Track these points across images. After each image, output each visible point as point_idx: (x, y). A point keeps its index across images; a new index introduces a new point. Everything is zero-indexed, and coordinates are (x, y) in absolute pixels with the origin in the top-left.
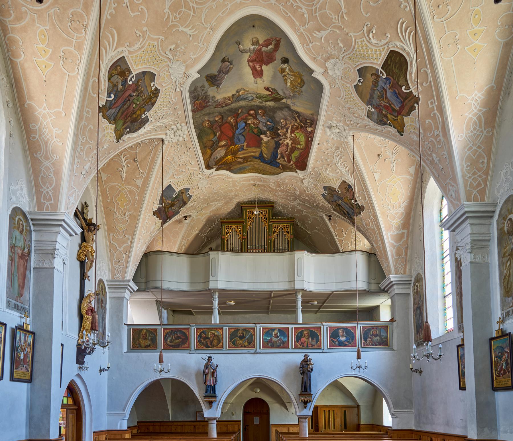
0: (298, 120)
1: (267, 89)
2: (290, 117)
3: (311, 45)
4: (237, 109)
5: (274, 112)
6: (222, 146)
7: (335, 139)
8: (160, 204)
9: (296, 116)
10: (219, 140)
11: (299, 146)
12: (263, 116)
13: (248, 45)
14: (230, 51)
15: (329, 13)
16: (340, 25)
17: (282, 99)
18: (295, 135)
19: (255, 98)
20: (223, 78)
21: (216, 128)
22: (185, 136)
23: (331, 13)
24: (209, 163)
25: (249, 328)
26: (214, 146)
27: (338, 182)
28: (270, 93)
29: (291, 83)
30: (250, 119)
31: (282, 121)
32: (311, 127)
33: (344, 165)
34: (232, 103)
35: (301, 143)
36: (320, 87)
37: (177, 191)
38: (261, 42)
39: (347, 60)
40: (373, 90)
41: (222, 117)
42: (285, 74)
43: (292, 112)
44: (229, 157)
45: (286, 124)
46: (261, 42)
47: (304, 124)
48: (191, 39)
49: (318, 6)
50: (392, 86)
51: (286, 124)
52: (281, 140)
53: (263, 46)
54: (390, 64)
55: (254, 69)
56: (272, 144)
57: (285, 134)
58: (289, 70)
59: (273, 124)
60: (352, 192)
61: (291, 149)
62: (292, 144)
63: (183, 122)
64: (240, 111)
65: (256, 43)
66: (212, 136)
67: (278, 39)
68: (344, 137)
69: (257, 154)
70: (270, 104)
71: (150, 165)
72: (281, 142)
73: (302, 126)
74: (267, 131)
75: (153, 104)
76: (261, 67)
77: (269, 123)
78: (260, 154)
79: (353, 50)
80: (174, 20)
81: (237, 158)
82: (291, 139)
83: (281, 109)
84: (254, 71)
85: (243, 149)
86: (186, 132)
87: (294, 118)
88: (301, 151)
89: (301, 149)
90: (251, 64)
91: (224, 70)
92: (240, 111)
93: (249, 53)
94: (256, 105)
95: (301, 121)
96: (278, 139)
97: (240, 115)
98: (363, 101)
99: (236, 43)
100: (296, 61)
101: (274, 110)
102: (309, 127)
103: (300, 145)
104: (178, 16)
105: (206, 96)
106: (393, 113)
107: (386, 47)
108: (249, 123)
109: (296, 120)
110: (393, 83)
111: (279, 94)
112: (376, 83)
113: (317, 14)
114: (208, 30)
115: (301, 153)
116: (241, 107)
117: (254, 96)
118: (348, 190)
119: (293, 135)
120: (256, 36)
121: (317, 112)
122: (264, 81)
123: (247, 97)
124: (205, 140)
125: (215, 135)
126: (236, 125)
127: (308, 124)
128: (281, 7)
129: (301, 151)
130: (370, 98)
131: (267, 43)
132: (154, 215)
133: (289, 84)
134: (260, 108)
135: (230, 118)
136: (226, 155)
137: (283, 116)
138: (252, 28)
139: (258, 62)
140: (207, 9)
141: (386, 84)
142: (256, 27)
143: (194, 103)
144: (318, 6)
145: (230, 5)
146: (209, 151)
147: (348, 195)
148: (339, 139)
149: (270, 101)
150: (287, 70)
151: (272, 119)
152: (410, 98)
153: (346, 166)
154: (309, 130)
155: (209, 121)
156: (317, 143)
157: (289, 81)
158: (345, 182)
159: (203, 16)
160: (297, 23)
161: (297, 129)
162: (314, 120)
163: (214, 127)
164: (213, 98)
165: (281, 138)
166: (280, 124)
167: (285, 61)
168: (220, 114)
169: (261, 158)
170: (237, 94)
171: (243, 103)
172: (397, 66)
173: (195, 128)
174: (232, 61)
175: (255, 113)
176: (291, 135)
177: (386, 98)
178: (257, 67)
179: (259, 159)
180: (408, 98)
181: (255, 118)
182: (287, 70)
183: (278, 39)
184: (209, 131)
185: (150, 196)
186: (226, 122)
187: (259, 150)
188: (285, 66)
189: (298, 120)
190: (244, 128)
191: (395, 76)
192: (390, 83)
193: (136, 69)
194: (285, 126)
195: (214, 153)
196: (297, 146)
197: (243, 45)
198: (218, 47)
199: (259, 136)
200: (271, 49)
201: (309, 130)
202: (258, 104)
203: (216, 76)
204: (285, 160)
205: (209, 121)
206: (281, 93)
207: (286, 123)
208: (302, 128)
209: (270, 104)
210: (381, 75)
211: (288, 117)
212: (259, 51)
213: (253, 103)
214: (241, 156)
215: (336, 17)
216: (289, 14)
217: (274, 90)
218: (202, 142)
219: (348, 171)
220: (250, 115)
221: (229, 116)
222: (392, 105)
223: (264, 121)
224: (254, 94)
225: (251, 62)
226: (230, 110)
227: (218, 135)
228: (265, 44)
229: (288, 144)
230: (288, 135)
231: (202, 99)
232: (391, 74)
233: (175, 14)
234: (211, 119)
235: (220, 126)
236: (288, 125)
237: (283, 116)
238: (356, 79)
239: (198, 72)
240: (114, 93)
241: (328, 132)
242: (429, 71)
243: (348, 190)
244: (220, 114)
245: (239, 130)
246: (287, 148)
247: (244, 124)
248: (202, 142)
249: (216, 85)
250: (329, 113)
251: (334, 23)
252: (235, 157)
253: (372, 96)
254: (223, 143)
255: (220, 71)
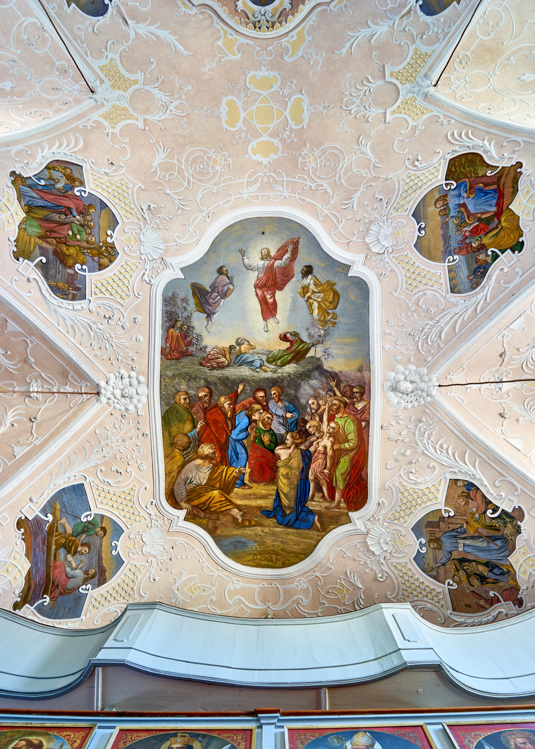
0: (338, 393)
1: (284, 338)
2: (323, 389)
3: (340, 226)
4: (235, 383)
5: (297, 387)
6: (205, 458)
7: (410, 406)
8: (44, 511)
9: (333, 384)
10: (200, 440)
11: (347, 445)
12: (279, 400)
13: (255, 259)
14: (230, 260)
15: (357, 171)
16: (374, 175)
17: (308, 350)
18: (337, 423)
19: (266, 364)
20: (217, 303)
21: (198, 411)
22: (140, 406)
23: (360, 170)
24: (176, 489)
26: (189, 450)
27: (441, 488)
28: (288, 345)
29: (320, 307)
30: (258, 410)
31: (310, 402)
32: (361, 400)
33: (441, 446)
34: (228, 366)
35: (350, 437)
36: (362, 287)
37: (94, 511)
38: (273, 254)
41: (211, 393)
42: (309, 294)
43: (326, 378)
44: (216, 493)
45: (319, 406)
46: (273, 254)
47: (349, 398)
48: (179, 212)
49: (342, 171)
51: (319, 406)
52: (311, 444)
53: (276, 260)
55: (263, 301)
56: (296, 462)
57: (318, 429)
58: (316, 285)
59: (295, 415)
60: (478, 495)
61: (333, 457)
62: (333, 444)
63: (143, 374)
64: (241, 387)
65: (266, 256)
66: (188, 426)
67: (296, 239)
68: (424, 394)
69: (268, 503)
70: (290, 368)
71: (58, 429)
72: (312, 449)
73: (346, 404)
74: (287, 433)
75: (98, 109)
76: (273, 296)
77: (289, 415)
78: (275, 500)
79: (398, 192)
80: (161, 177)
81: (232, 503)
82: (331, 435)
83: (306, 376)
84: (264, 307)
85: (243, 484)
86: (144, 399)
87: (331, 390)
88: (352, 454)
89: (352, 450)
90: (259, 292)
91: (220, 289)
92: (241, 387)
93: (257, 273)
94: (268, 379)
95: (343, 394)
96: (307, 443)
97: (240, 398)
99: (240, 251)
100: (322, 265)
101: (295, 381)
102: (359, 402)
103: (348, 441)
104: (167, 177)
105: (189, 327)
106: (491, 227)
107: (442, 161)
108: (255, 421)
109: (335, 395)
111: (302, 342)
113: (343, 181)
114: (204, 214)
115: (352, 460)
116: (243, 380)
117: (264, 358)
118: (468, 496)
119: (332, 425)
120: (267, 246)
121: (365, 366)
122: (278, 323)
123: (253, 361)
124: (174, 430)
125: (195, 427)
126: (233, 418)
127: (353, 393)
128: (297, 196)
129: (352, 454)
131: (282, 252)
132: (19, 529)
133: (316, 312)
134: (274, 382)
135: (222, 399)
136: (210, 485)
137: (311, 392)
138: (261, 235)
139: (269, 288)
140: (205, 189)
142: (267, 234)
143: (168, 331)
144: (342, 171)
145: (234, 197)
146: (178, 457)
147: (473, 507)
148: (416, 404)
149: (289, 362)
150: (312, 287)
151: (294, 404)
152: (505, 173)
153: (445, 446)
154: (360, 406)
155: (187, 393)
156: (379, 427)
157: (316, 304)
158: (457, 480)
159: (199, 196)
160: (319, 205)
161: (338, 410)
162: (365, 383)
163: (194, 409)
164: (199, 337)
165: (314, 438)
166: (309, 410)
167: (308, 271)
168: (208, 385)
169: (276, 512)
170: (238, 348)
171: (245, 371)
173: (161, 398)
174: (232, 278)
175: (265, 396)
176: (328, 425)
177: (469, 215)
178: (268, 297)
179: (275, 516)
181: (266, 408)
182: (312, 287)
183: (295, 241)
184: (186, 415)
185: (30, 478)
186: (216, 406)
187: (271, 489)
188: (309, 280)
189: (338, 393)
190: (247, 429)
193: (93, 279)
194: (316, 411)
195: (188, 467)
196: (342, 446)
197: (248, 258)
198: (214, 245)
199: (272, 451)
200: (286, 260)
201: (360, 406)
202: (269, 375)
203: (208, 292)
204: (323, 496)
205: (187, 393)
206: (305, 338)
207: (318, 404)
208: (347, 406)
209: (290, 368)
211: (321, 392)
212: (270, 269)
213: (263, 375)
214: (239, 502)
215: (367, 171)
216: (307, 200)
217: (295, 334)
218: (170, 433)
219: (454, 456)
220: (258, 402)
221: (221, 395)
223: (280, 412)
224: (264, 354)
225: (260, 288)
226: (225, 381)
227: (199, 426)
228: (278, 256)
229: (325, 447)
230: (325, 427)
231: (181, 328)
232: (461, 177)
233: (164, 173)
234: (192, 392)
235: (205, 410)
236: (323, 407)
237: (311, 392)
238: (414, 228)
239: (183, 270)
240: (47, 183)
241: (394, 398)
243: (468, 496)
244: (208, 385)
245: (236, 431)
246: (325, 459)
247: (246, 420)
248: (170, 433)
249: (205, 312)
250: (387, 346)
251: (365, 178)
252: (227, 499)
254: (206, 449)
255: (214, 287)
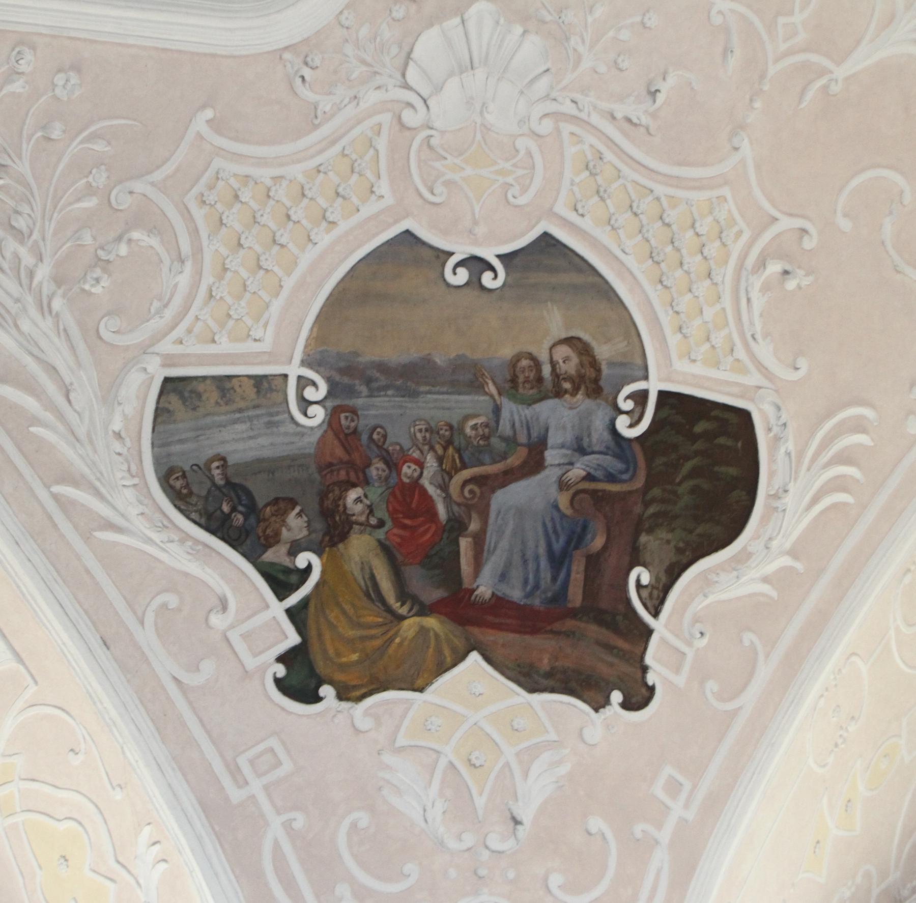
25: (383, 230)
39: (571, 150)
40: (467, 376)
50: (599, 498)
54: (694, 438)
98: (323, 317)
110: (623, 497)
112: (527, 380)
130: (382, 367)
141: (581, 450)
152: (621, 643)
172: (704, 484)
177: (488, 484)
180: (616, 630)
191: (656, 492)
192: (611, 478)
210: (628, 405)
222: (465, 543)
232: (660, 461)
242: (765, 671)
253: (412, 377)
